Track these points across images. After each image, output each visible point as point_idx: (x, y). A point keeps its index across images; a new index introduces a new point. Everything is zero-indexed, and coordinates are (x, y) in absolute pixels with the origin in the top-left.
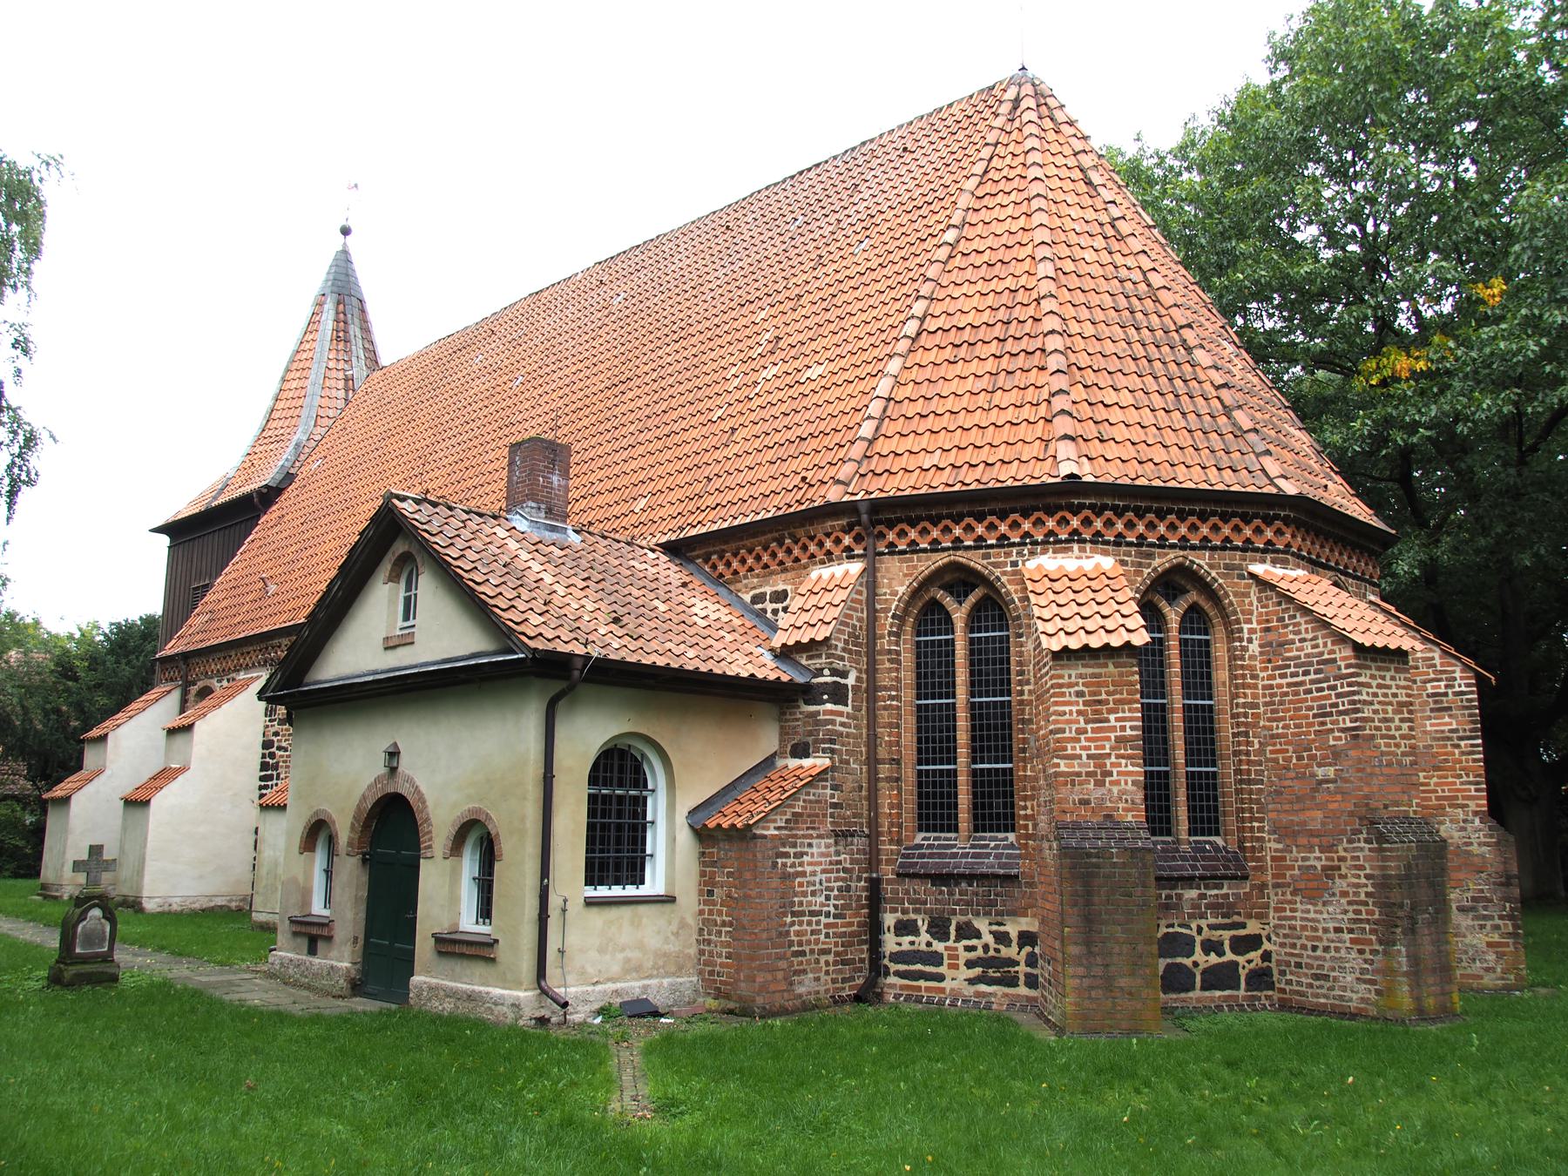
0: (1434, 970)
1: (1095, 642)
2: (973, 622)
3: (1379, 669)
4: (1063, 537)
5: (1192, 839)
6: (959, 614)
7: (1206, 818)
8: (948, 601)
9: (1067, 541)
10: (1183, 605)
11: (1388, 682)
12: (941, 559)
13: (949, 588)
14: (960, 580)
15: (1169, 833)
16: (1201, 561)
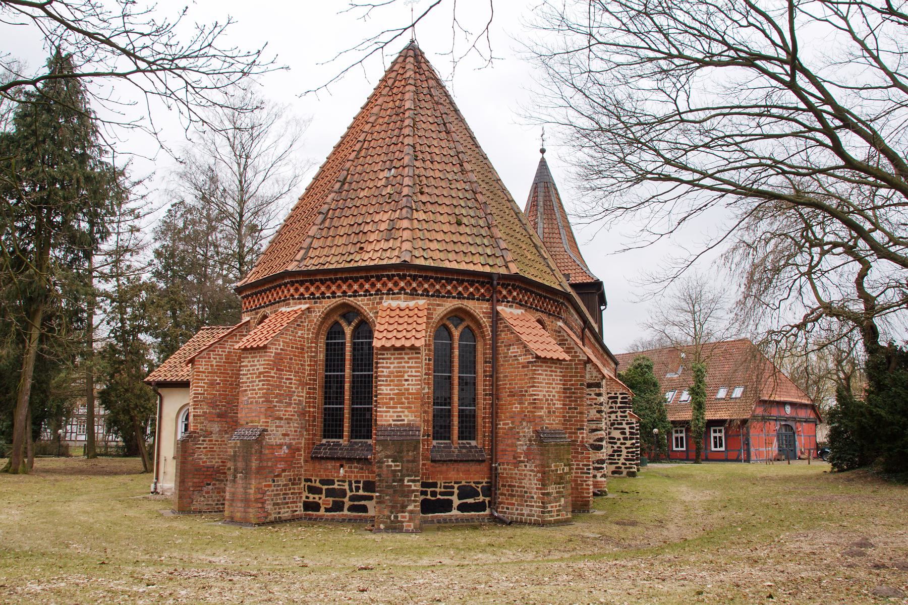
0: (242, 501)
1: (398, 344)
2: (355, 334)
3: (252, 357)
4: (396, 291)
5: (460, 442)
6: (348, 330)
7: (468, 429)
8: (344, 324)
9: (398, 293)
10: (460, 328)
11: (256, 363)
12: (338, 301)
13: (344, 316)
14: (348, 312)
15: (449, 439)
16: (470, 305)
